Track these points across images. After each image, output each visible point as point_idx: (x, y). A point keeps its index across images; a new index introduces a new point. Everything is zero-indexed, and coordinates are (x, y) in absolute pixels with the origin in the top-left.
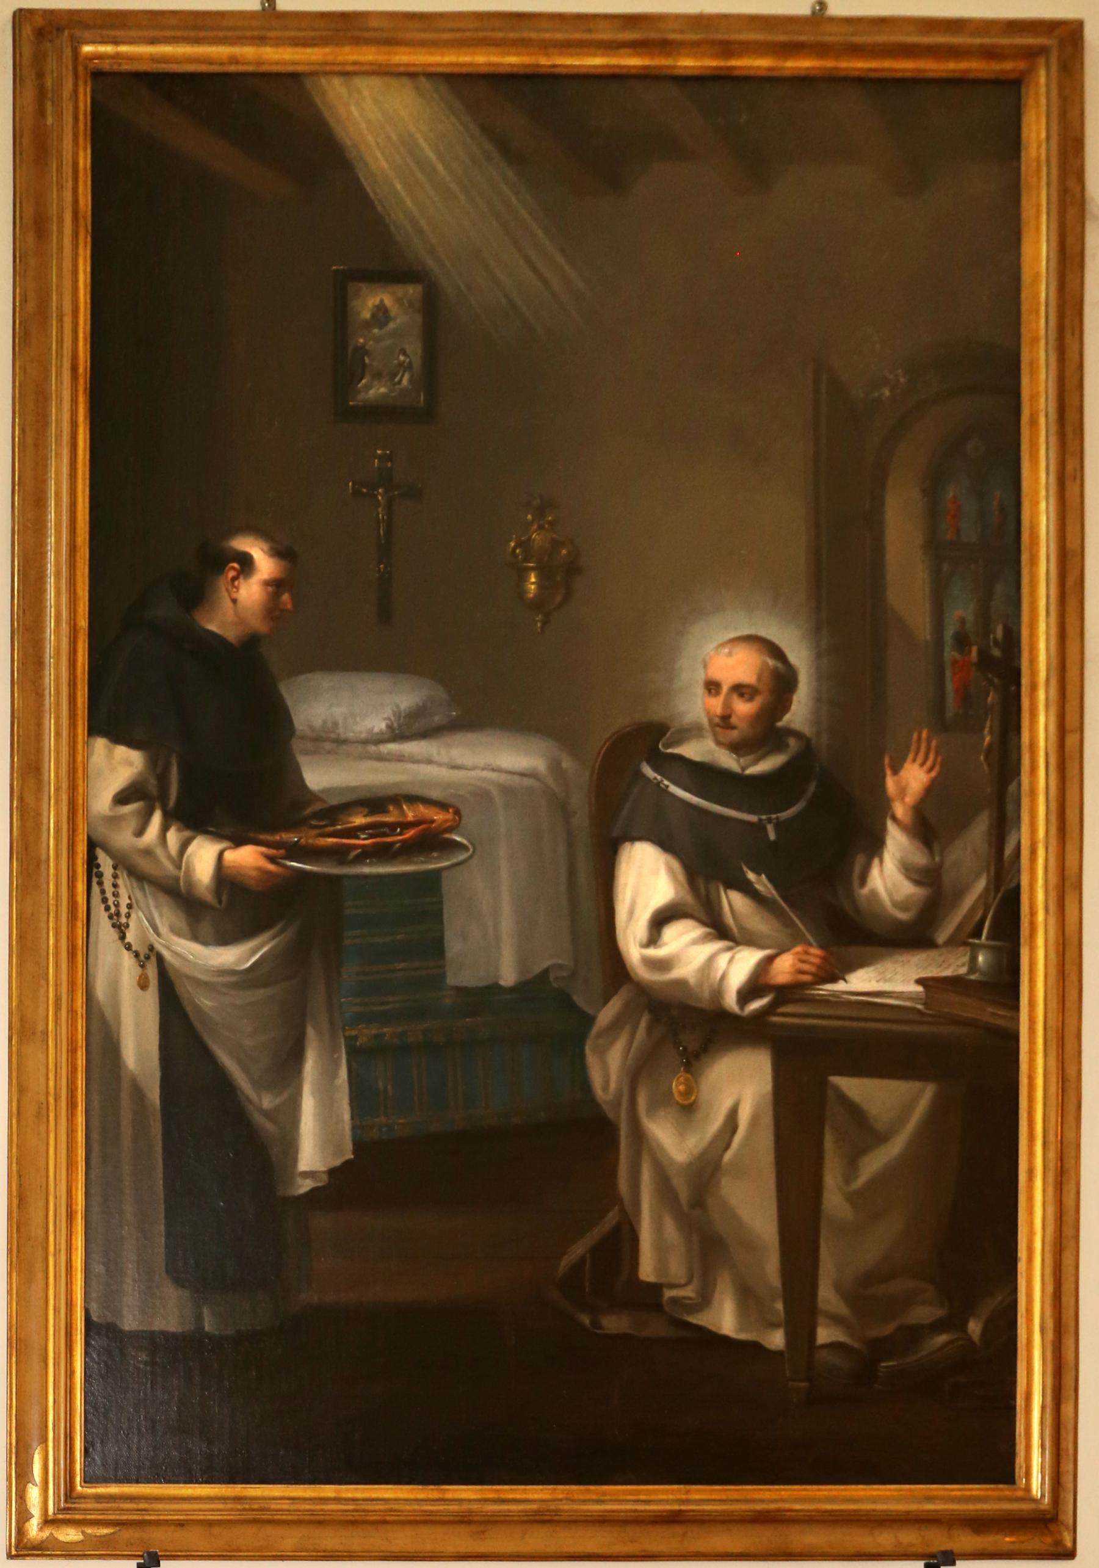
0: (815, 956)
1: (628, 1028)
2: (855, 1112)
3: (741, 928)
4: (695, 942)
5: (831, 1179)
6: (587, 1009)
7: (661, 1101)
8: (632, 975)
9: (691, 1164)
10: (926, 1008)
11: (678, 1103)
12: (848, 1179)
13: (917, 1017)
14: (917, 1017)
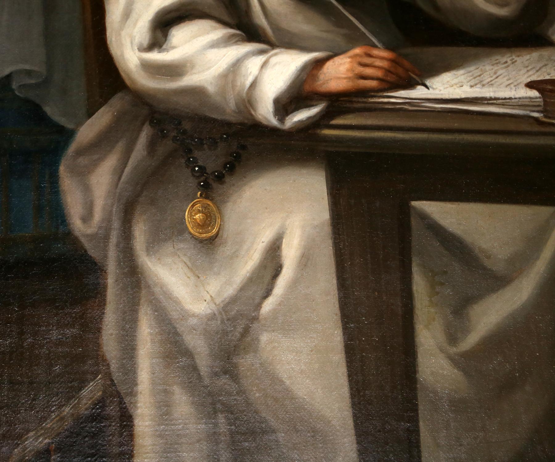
0: (382, 58)
1: (120, 147)
2: (454, 246)
3: (276, 28)
4: (214, 45)
5: (429, 339)
6: (70, 126)
7: (168, 232)
8: (128, 82)
9: (212, 317)
10: (545, 117)
11: (193, 236)
12: (453, 338)
13: (537, 128)
14: (537, 128)
